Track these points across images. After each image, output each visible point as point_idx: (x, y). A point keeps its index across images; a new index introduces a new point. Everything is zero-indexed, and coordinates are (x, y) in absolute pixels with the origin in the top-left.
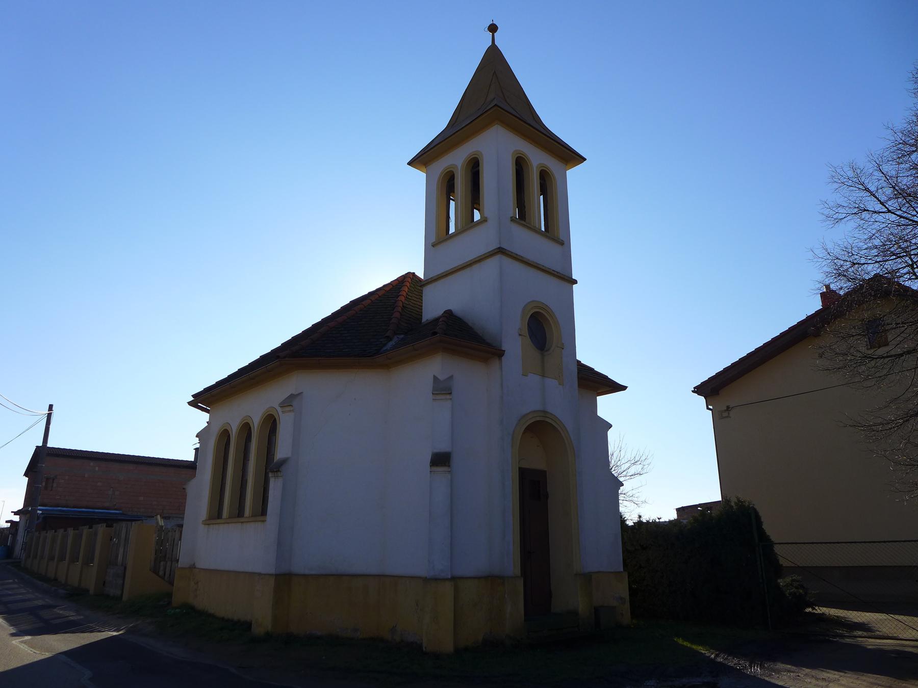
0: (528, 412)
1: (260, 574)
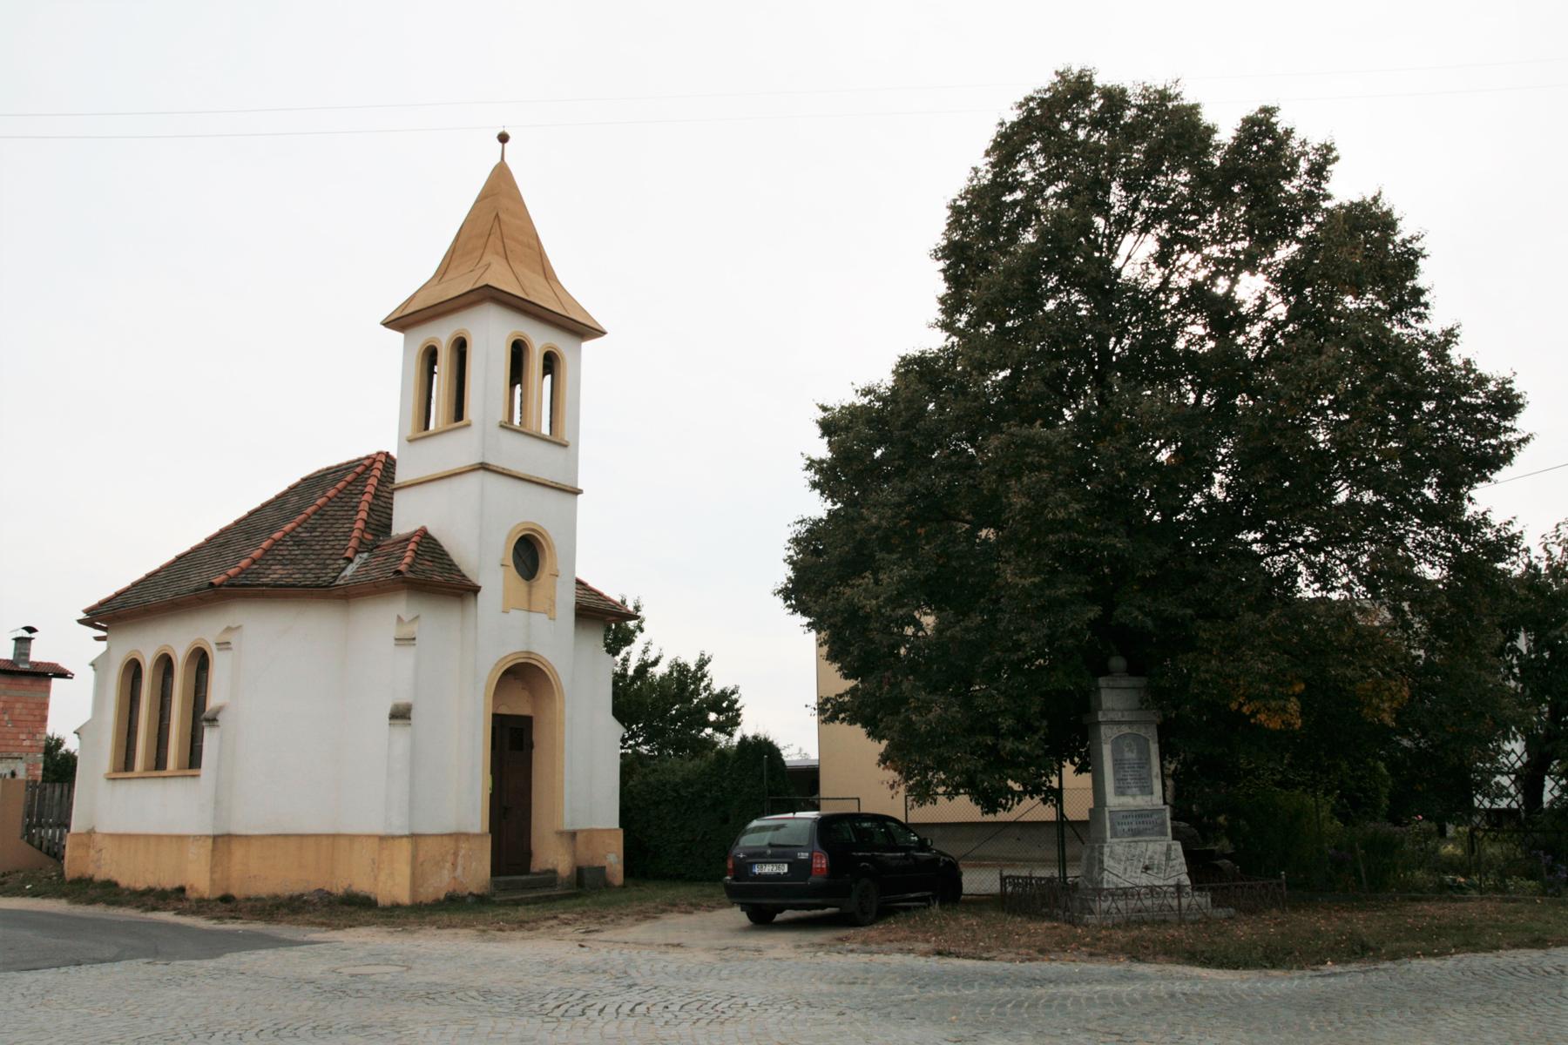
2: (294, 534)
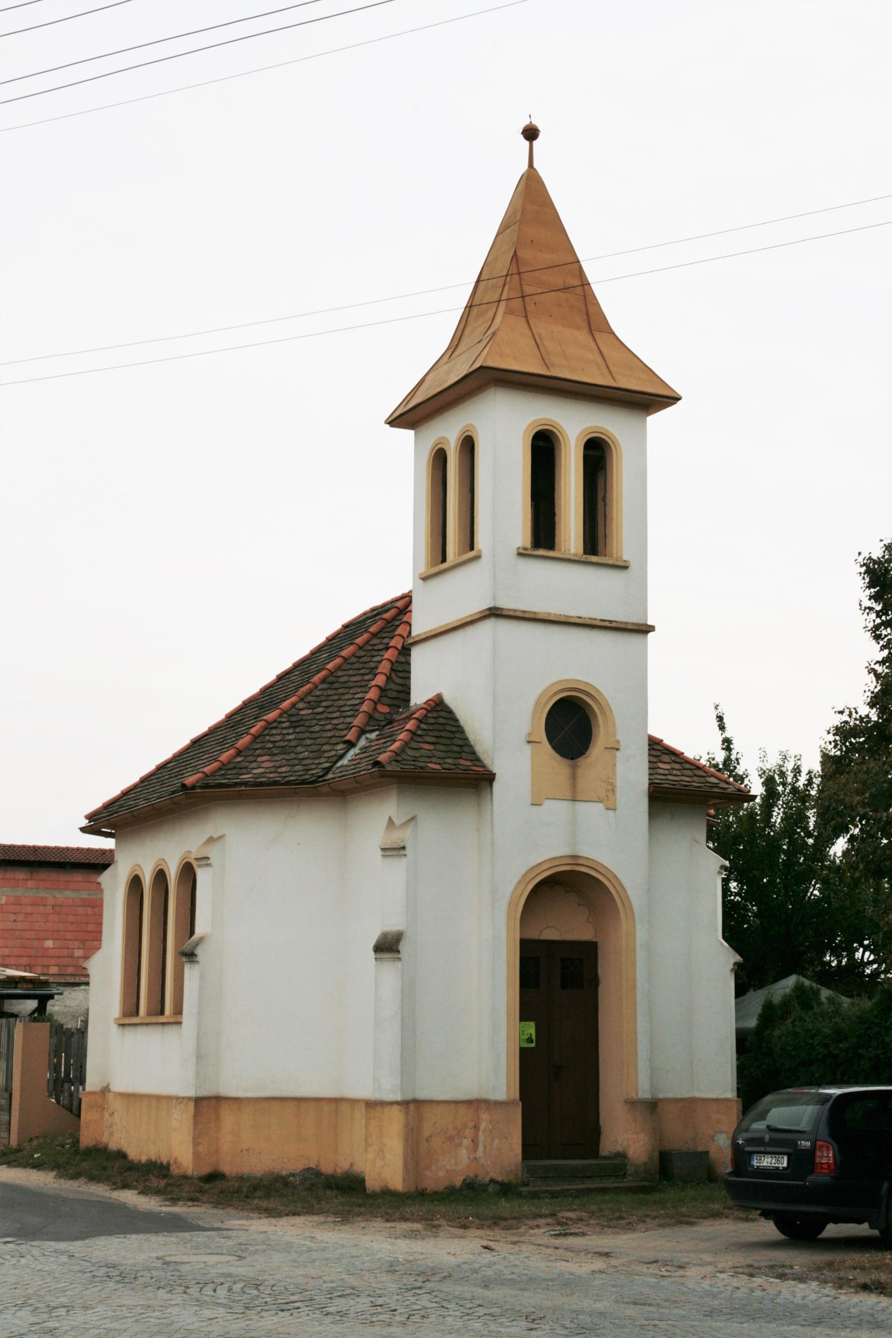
0: (541, 861)
1: (178, 1098)
2: (294, 711)
